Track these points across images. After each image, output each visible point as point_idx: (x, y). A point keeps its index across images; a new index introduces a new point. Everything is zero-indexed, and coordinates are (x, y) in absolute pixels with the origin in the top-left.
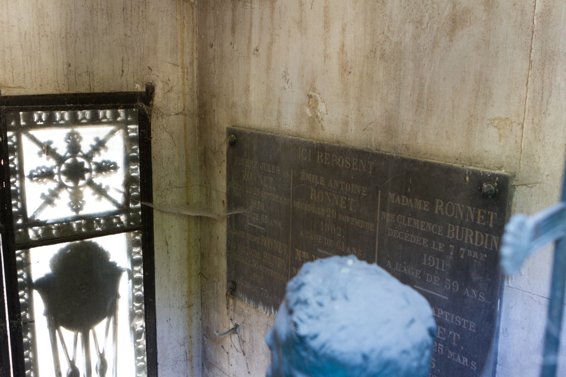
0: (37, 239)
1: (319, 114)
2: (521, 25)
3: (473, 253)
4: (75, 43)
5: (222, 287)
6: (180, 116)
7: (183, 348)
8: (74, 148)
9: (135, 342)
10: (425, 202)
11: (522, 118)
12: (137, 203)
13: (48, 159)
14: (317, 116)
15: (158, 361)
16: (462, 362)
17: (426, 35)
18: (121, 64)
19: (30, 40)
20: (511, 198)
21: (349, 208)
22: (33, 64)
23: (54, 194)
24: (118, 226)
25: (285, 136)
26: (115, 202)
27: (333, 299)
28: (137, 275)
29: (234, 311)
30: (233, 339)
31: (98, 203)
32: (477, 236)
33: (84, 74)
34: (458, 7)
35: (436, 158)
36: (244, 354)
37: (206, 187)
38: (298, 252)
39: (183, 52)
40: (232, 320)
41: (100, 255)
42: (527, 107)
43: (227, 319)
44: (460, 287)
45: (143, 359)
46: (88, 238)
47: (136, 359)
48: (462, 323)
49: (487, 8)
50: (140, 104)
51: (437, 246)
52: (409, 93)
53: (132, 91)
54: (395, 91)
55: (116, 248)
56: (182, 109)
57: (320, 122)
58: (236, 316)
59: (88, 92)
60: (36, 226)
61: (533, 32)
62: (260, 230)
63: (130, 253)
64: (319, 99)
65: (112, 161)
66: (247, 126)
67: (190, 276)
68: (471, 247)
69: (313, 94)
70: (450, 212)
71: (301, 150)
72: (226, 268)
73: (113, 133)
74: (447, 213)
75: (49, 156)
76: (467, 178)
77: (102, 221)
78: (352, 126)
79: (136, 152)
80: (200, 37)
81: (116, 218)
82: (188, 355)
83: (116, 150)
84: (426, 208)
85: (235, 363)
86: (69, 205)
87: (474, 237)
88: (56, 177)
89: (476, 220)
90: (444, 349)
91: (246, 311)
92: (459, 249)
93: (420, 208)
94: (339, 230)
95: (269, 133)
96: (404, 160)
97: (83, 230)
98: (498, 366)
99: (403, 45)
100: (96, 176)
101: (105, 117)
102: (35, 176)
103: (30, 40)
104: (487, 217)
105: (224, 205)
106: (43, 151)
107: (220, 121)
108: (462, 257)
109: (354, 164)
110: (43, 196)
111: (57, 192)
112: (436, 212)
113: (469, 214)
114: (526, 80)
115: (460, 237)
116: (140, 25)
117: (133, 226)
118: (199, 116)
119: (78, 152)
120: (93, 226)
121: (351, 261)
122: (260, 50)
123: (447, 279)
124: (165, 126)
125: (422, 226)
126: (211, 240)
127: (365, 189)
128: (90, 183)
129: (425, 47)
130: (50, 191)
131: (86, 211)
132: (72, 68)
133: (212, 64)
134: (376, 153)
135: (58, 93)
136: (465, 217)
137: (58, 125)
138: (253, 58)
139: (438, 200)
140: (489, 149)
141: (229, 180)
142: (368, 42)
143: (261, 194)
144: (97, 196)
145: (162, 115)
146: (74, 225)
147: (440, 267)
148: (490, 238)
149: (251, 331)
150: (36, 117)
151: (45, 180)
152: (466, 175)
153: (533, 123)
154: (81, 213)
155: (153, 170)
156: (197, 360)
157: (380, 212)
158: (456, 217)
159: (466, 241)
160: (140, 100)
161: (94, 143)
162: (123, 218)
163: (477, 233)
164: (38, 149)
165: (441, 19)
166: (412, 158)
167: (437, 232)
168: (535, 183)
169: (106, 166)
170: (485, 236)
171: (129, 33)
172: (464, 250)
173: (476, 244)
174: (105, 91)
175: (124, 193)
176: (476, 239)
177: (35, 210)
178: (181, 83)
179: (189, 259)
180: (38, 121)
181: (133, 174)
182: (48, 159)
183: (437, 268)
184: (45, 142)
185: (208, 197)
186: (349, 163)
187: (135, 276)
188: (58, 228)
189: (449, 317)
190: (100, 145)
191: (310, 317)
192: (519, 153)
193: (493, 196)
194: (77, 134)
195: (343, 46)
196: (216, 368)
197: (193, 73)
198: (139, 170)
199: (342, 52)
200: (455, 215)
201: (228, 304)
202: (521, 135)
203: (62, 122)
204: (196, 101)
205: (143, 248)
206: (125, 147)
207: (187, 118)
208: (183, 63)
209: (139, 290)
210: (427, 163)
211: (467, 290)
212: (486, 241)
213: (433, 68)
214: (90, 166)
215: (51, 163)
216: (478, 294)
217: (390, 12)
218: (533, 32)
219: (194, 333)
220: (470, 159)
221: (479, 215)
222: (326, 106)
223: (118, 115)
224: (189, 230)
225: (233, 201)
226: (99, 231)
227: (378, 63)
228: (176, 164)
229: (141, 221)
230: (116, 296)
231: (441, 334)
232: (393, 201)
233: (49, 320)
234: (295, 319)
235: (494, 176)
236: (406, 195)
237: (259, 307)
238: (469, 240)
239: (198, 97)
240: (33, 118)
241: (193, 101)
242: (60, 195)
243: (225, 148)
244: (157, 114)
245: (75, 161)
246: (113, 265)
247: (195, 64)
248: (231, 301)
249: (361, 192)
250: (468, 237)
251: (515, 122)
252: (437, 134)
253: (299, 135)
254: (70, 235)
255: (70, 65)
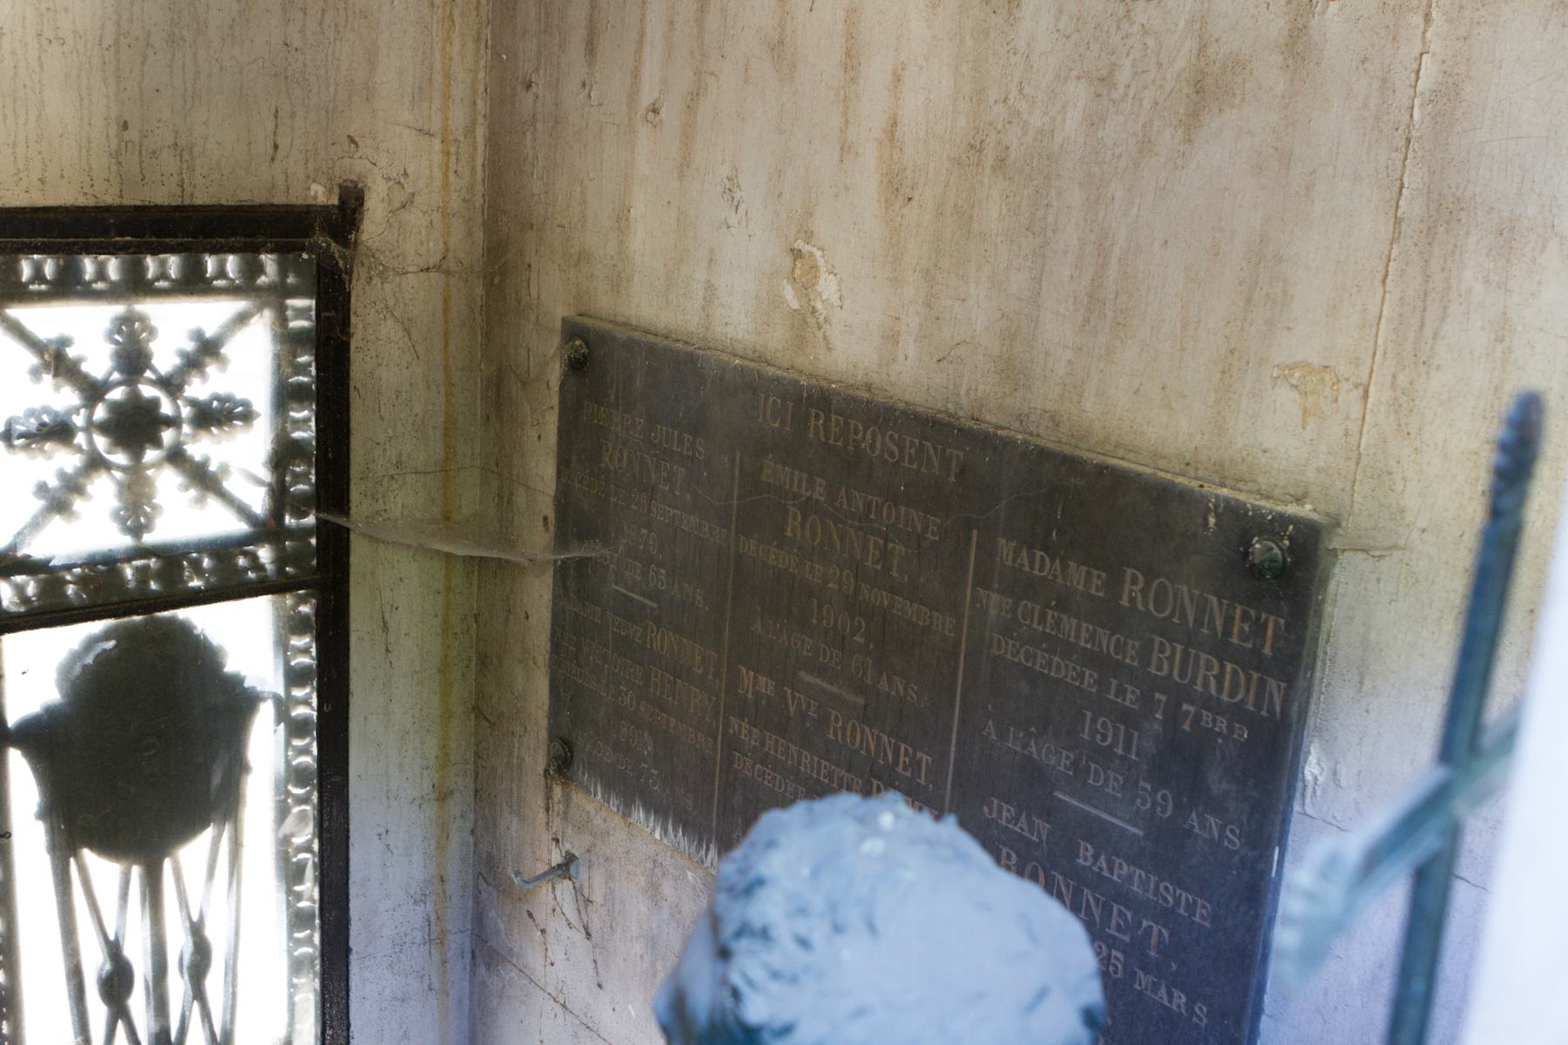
0: (22, 609)
1: (819, 305)
2: (1377, 118)
3: (1214, 720)
4: (143, 63)
5: (534, 751)
6: (433, 275)
7: (420, 909)
8: (133, 360)
9: (289, 892)
10: (1095, 572)
11: (1367, 371)
12: (305, 515)
13: (57, 388)
14: (814, 311)
15: (351, 944)
16: (1170, 1002)
17: (1122, 118)
18: (270, 126)
19: (14, 53)
20: (1324, 582)
21: (890, 569)
22: (22, 120)
23: (73, 486)
24: (251, 575)
25: (725, 357)
26: (243, 511)
27: (838, 929)
28: (300, 711)
29: (565, 816)
30: (558, 893)
31: (66, 331)
32: (1228, 676)
33: (165, 152)
34: (1211, 50)
35: (1131, 456)
36: (588, 935)
37: (500, 474)
38: (747, 675)
39: (447, 96)
40: (557, 841)
41: (198, 657)
42: (1380, 342)
43: (546, 837)
44: (1177, 805)
45: (310, 938)
46: (166, 609)
47: (290, 937)
48: (1177, 901)
49: (1290, 62)
50: (322, 240)
51: (1121, 692)
52: (1067, 273)
53: (300, 202)
54: (1029, 264)
55: (246, 638)
56: (439, 256)
57: (820, 328)
58: (569, 832)
59: (176, 202)
60: (20, 573)
61: (1408, 141)
62: (644, 605)
63: (282, 645)
64: (821, 262)
65: (239, 396)
66: (620, 319)
67: (446, 715)
68: (1208, 703)
69: (806, 248)
70: (1160, 606)
71: (766, 399)
72: (547, 702)
73: (242, 319)
74: (1151, 607)
75: (60, 379)
76: (1212, 520)
77: (206, 562)
78: (908, 345)
79: (308, 374)
80: (497, 55)
81: (245, 554)
82: (433, 927)
83: (251, 363)
84: (1098, 590)
85: (562, 956)
86: (116, 516)
87: (1220, 678)
88: (80, 439)
89: (1227, 632)
90: (1125, 966)
91: (598, 821)
92: (1179, 705)
93: (1081, 587)
94: (859, 627)
95: (679, 345)
96: (1044, 454)
97: (153, 586)
98: (1264, 1018)
99: (1058, 138)
100: (194, 437)
101: (221, 273)
102: (21, 436)
103: (14, 53)
104: (1260, 628)
105: (547, 529)
106: (46, 366)
107: (543, 298)
108: (1186, 727)
109: (907, 451)
110: (42, 489)
111: (81, 480)
112: (1125, 602)
113: (1212, 616)
114: (1382, 268)
115: (1182, 675)
116: (327, 18)
117: (293, 577)
118: (485, 277)
119: (142, 371)
120: (181, 576)
121: (892, 814)
122: (663, 111)
123: (1142, 783)
124: (391, 302)
125: (1084, 635)
126: (507, 620)
127: (934, 523)
128: (176, 457)
129: (1117, 151)
130: (63, 476)
131: (163, 532)
132: (133, 134)
133: (529, 136)
134: (971, 430)
135: (91, 202)
136: (1199, 622)
137: (87, 293)
138: (643, 131)
139: (1129, 572)
140: (1272, 443)
141: (563, 464)
142: (962, 121)
143: (650, 511)
144: (193, 492)
145: (382, 273)
146: (129, 572)
147: (1127, 749)
148: (1262, 683)
149: (610, 877)
150: (26, 270)
151: (48, 446)
152: (1208, 511)
153: (1393, 386)
154: (149, 539)
155: (353, 424)
156: (458, 941)
157: (974, 587)
158: (1175, 620)
159: (1199, 688)
160: (322, 229)
161: (190, 346)
162: (265, 554)
163: (1229, 667)
164: (32, 360)
165: (1164, 79)
166: (1068, 450)
167: (1124, 657)
168: (1390, 548)
169: (220, 411)
170: (1249, 678)
171: (296, 41)
172: (1192, 709)
173: (1225, 697)
174: (224, 202)
175: (270, 485)
176: (1227, 684)
177: (18, 529)
178: (437, 183)
179: (444, 668)
180: (32, 281)
181: (297, 435)
182: (57, 388)
183: (1120, 752)
184: (50, 341)
185: (505, 501)
186: (895, 449)
187: (293, 714)
188: (81, 581)
189: (1144, 883)
190: (206, 350)
191: (775, 975)
192: (1352, 464)
193: (1275, 574)
194: (142, 319)
195: (895, 124)
196: (509, 967)
197: (473, 157)
198: (313, 424)
199: (892, 139)
200: (1172, 615)
201: (548, 797)
202: (1360, 416)
203: (100, 286)
204: (479, 236)
205: (319, 639)
206: (277, 357)
207: (452, 281)
208: (445, 129)
209: (305, 751)
210: (1107, 467)
211: (1194, 815)
212: (1252, 692)
213: (1135, 211)
214: (177, 408)
215: (65, 398)
216: (1222, 828)
217: (1029, 45)
218: (1408, 141)
219: (453, 869)
220: (1222, 466)
221: (1237, 622)
222: (839, 284)
223: (260, 270)
224: (449, 589)
225: (573, 520)
226: (197, 591)
227: (986, 181)
228: (418, 408)
229: (314, 562)
230: (237, 766)
231: (1119, 925)
232: (1009, 563)
233: (52, 832)
234: (736, 979)
235: (1283, 520)
236: (1045, 548)
237: (635, 815)
238: (1206, 685)
239: (484, 224)
240: (18, 273)
241: (470, 234)
242: (90, 488)
243: (555, 373)
244: (370, 268)
245: (135, 396)
246: (235, 682)
247: (481, 132)
248: (558, 791)
249: (925, 529)
250: (1206, 677)
251: (1347, 380)
252: (1137, 391)
253: (761, 359)
254: (115, 599)
255: (125, 126)
